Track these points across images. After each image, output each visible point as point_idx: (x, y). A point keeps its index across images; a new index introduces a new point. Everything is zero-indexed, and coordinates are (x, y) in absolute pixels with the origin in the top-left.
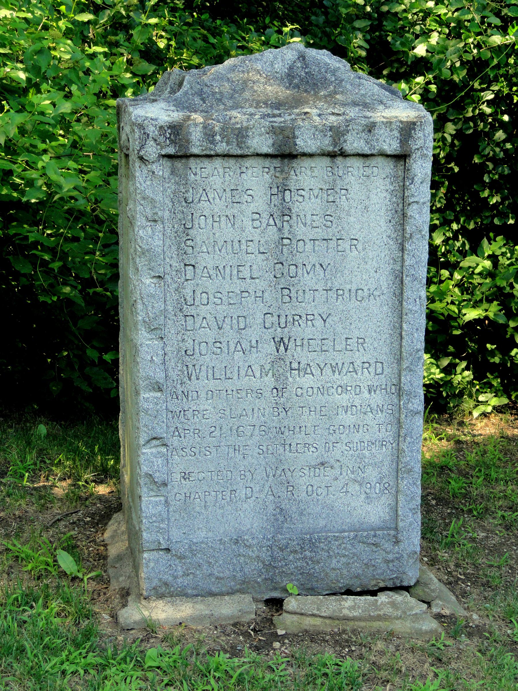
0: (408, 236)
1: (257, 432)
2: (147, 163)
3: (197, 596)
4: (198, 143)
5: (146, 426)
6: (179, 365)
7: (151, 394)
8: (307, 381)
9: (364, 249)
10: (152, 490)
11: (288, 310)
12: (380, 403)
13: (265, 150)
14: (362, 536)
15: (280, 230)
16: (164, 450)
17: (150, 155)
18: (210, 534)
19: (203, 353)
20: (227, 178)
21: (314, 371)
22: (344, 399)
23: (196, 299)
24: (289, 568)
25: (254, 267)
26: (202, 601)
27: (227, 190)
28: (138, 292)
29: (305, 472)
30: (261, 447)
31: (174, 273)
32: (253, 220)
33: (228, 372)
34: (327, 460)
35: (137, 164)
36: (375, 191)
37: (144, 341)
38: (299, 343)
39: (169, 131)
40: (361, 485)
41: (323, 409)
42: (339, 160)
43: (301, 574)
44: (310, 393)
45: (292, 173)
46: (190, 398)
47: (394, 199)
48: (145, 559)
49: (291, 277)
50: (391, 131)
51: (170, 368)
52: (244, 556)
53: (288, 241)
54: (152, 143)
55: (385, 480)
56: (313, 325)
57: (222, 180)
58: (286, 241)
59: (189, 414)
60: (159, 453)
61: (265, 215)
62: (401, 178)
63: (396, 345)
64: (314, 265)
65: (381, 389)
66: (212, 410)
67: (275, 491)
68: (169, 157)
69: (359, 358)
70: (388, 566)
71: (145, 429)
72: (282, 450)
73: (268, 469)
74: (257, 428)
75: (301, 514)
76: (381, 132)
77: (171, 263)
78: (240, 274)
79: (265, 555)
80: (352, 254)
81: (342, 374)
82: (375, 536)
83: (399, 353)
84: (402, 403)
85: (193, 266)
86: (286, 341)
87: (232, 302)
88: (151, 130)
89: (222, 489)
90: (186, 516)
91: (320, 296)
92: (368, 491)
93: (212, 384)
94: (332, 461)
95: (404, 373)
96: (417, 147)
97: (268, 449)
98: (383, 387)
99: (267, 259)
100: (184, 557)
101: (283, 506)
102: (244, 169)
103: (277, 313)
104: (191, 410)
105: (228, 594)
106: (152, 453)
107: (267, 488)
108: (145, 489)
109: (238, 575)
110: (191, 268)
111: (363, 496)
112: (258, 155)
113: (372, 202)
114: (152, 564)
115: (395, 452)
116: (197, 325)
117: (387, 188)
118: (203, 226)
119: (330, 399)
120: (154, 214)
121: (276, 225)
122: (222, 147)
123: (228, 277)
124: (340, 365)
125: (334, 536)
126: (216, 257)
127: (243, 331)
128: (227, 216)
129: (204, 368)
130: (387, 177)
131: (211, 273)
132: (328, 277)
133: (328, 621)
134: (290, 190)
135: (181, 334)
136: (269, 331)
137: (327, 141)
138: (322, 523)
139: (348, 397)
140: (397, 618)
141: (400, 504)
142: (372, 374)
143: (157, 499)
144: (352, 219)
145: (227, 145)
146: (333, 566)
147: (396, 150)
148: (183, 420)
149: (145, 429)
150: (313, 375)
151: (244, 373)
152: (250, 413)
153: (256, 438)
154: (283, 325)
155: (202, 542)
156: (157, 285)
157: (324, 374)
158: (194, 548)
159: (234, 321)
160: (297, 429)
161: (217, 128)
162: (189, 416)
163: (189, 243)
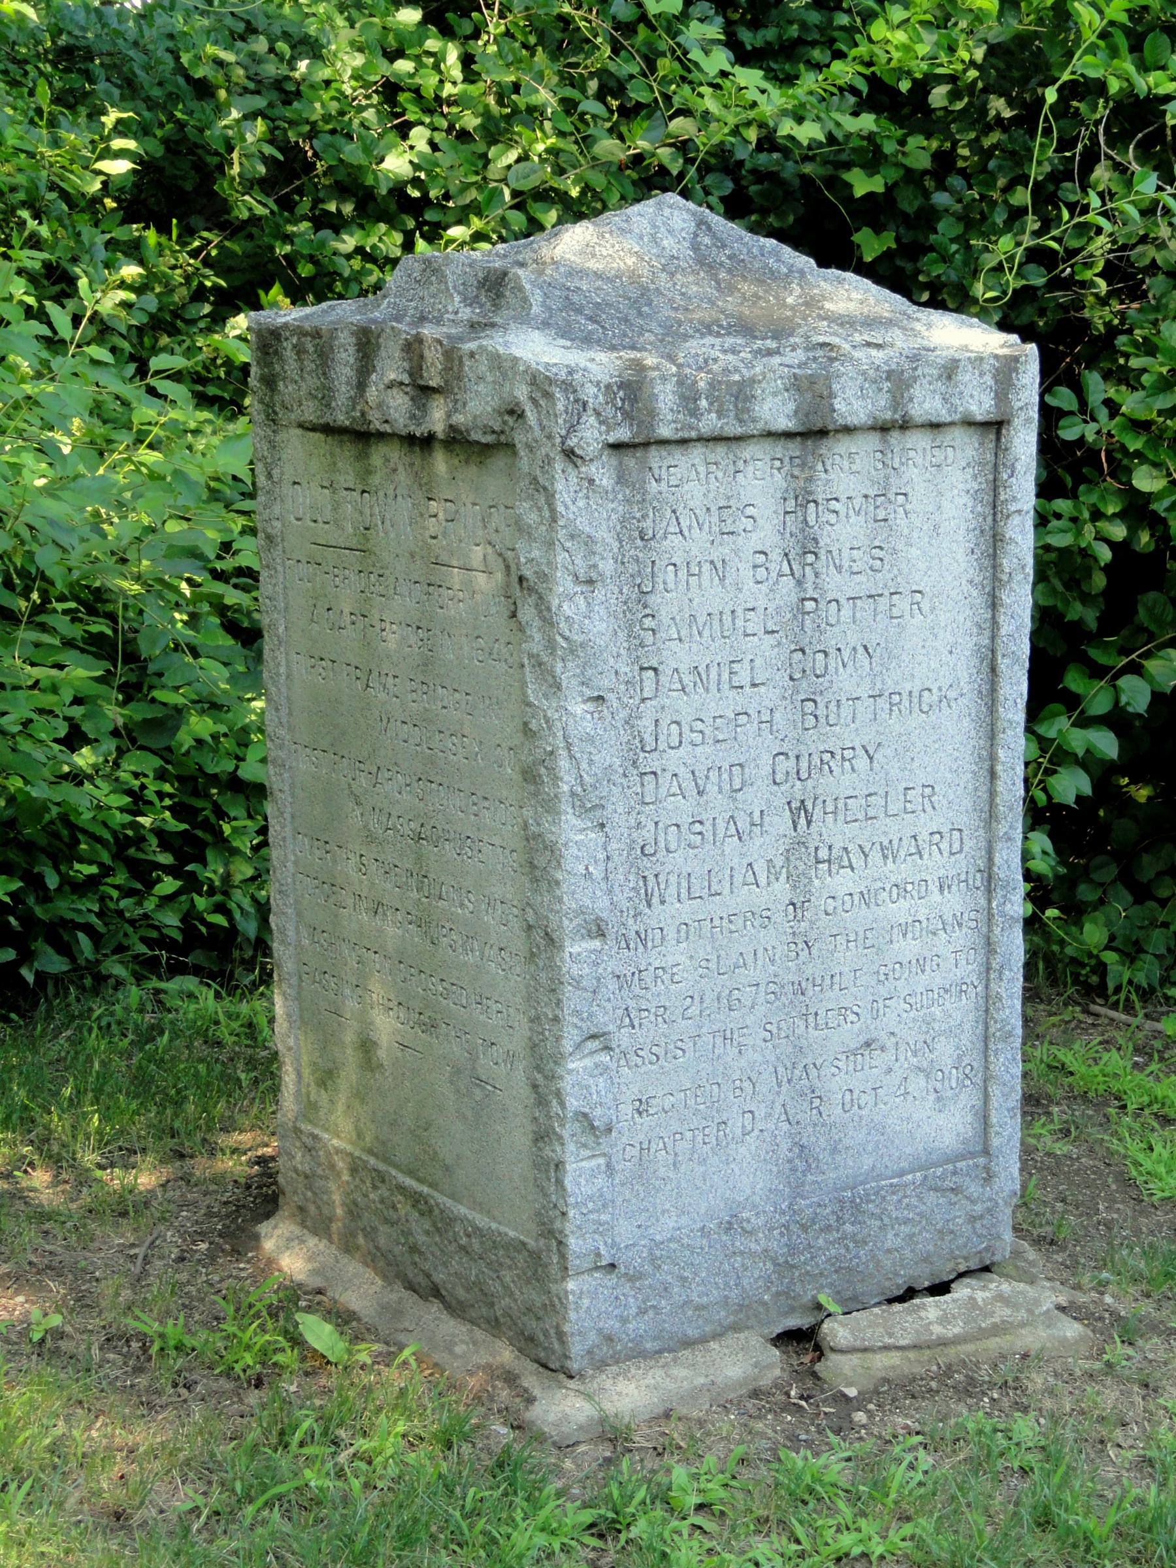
0: (1005, 578)
1: (761, 998)
2: (579, 462)
3: (660, 1352)
4: (669, 417)
5: (577, 1013)
6: (631, 878)
7: (584, 945)
8: (843, 882)
9: (933, 609)
10: (585, 1146)
11: (814, 743)
12: (958, 909)
13: (784, 423)
14: (935, 1177)
15: (799, 583)
16: (604, 1058)
17: (588, 444)
18: (684, 1220)
19: (672, 847)
20: (714, 485)
21: (854, 861)
22: (900, 911)
23: (662, 738)
24: (817, 1264)
25: (758, 662)
26: (675, 1360)
27: (713, 509)
28: (560, 734)
29: (840, 1064)
30: (768, 1027)
31: (623, 687)
32: (755, 567)
33: (714, 880)
34: (875, 1035)
35: (558, 466)
36: (949, 495)
37: (571, 836)
38: (830, 809)
39: (621, 394)
40: (927, 1077)
41: (868, 933)
42: (895, 437)
43: (836, 1271)
44: (848, 906)
45: (820, 467)
46: (650, 944)
47: (979, 509)
48: (573, 1292)
49: (818, 677)
50: (981, 375)
51: (616, 887)
52: (742, 1253)
53: (813, 603)
54: (592, 420)
55: (966, 1061)
56: (853, 769)
57: (703, 489)
58: (810, 605)
59: (648, 977)
60: (597, 1066)
61: (776, 555)
62: (990, 466)
63: (983, 793)
64: (854, 649)
65: (960, 882)
66: (688, 962)
67: (791, 1112)
68: (617, 447)
69: (926, 824)
70: (974, 1228)
71: (575, 1020)
72: (802, 1024)
73: (781, 1069)
74: (762, 988)
75: (835, 1151)
76: (967, 378)
77: (617, 667)
78: (735, 678)
79: (776, 1246)
80: (913, 621)
81: (898, 861)
82: (954, 1173)
83: (987, 808)
84: (994, 904)
85: (655, 670)
86: (810, 807)
87: (721, 737)
88: (589, 392)
89: (704, 1123)
90: (641, 1189)
91: (864, 708)
92: (939, 1086)
93: (686, 910)
94: (883, 1036)
95: (999, 846)
96: (1020, 404)
97: (779, 1029)
98: (963, 877)
99: (779, 644)
100: (640, 1276)
101: (804, 1141)
102: (740, 464)
103: (796, 752)
104: (651, 969)
105: (716, 1336)
106: (585, 1068)
107: (778, 1109)
108: (571, 1147)
109: (733, 1295)
110: (651, 673)
111: (932, 1097)
112: (770, 435)
113: (945, 516)
114: (586, 1302)
115: (981, 1001)
116: (663, 791)
117: (968, 486)
118: (671, 586)
119: (880, 911)
120: (590, 567)
121: (792, 574)
122: (710, 423)
123: (713, 687)
124: (895, 843)
125: (891, 1185)
126: (694, 645)
127: (739, 795)
128: (712, 562)
129: (673, 879)
130: (968, 464)
131: (686, 681)
132: (877, 669)
133: (911, 1355)
134: (815, 502)
135: (634, 814)
136: (783, 788)
137: (883, 400)
138: (867, 1162)
139: (907, 905)
140: (1023, 1325)
141: (994, 1103)
142: (946, 854)
143: (593, 1163)
144: (914, 552)
145: (719, 418)
146: (888, 1245)
147: (989, 413)
148: (637, 991)
149: (575, 1020)
150: (852, 869)
151: (741, 880)
152: (750, 959)
153: (761, 1009)
154: (804, 775)
155: (670, 1240)
156: (596, 715)
157: (870, 864)
158: (658, 1253)
159: (725, 776)
160: (828, 981)
161: (702, 384)
162: (648, 980)
163: (648, 622)
